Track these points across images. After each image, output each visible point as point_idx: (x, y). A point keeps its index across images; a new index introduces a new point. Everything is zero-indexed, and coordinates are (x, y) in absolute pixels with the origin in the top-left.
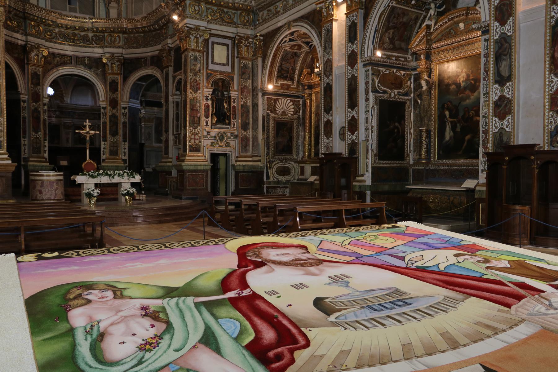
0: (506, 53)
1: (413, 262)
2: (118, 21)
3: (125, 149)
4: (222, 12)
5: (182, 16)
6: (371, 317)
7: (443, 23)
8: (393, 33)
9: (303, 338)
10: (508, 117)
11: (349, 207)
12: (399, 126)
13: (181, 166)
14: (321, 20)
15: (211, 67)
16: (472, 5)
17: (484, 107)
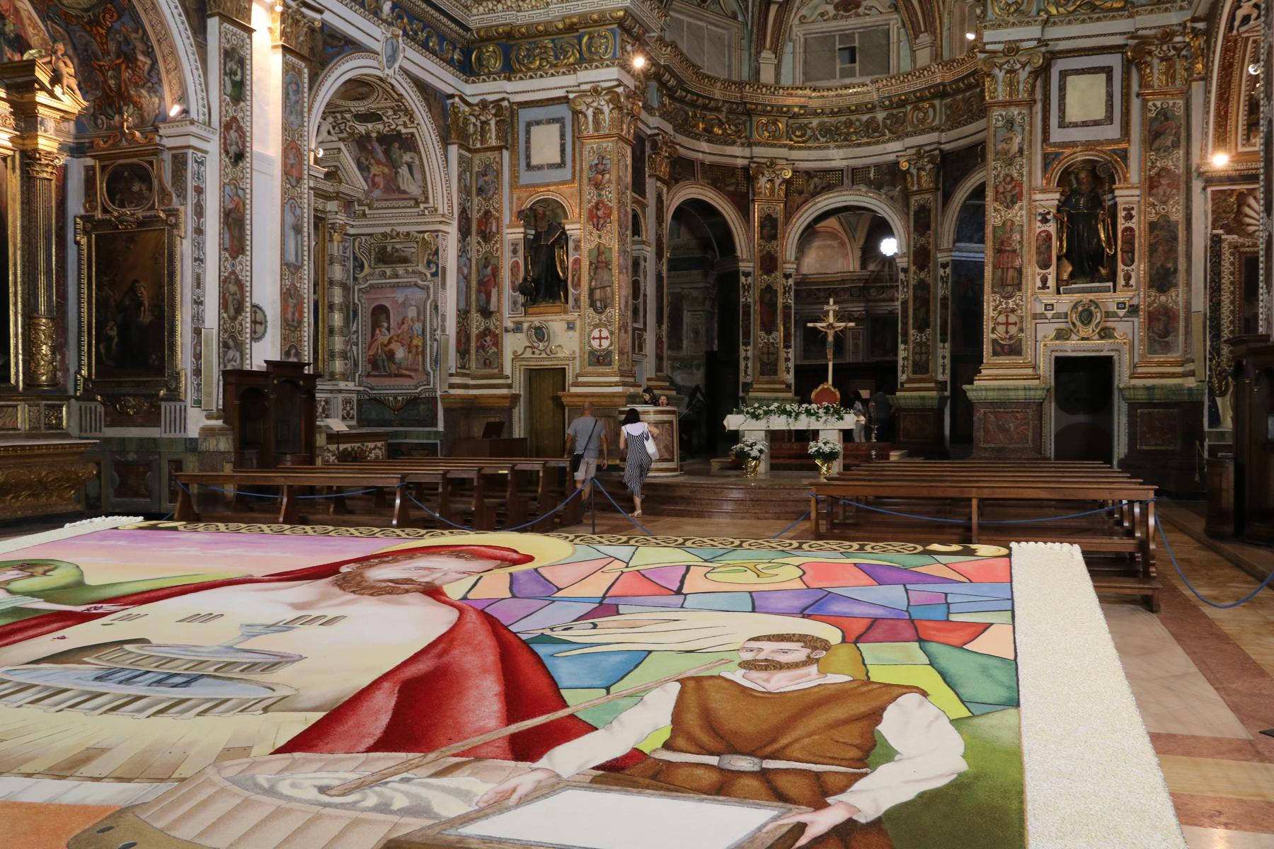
2: (926, 72)
3: (944, 357)
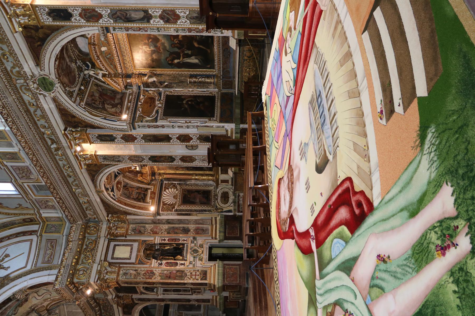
0: (125, 14)
1: (291, 89)
4: (86, 250)
5: (88, 286)
6: (330, 124)
7: (101, 64)
8: (108, 104)
9: (345, 183)
10: (178, 13)
11: (251, 142)
12: (186, 100)
13: (218, 288)
14: (96, 165)
15: (133, 260)
16: (87, 40)
17: (169, 31)
